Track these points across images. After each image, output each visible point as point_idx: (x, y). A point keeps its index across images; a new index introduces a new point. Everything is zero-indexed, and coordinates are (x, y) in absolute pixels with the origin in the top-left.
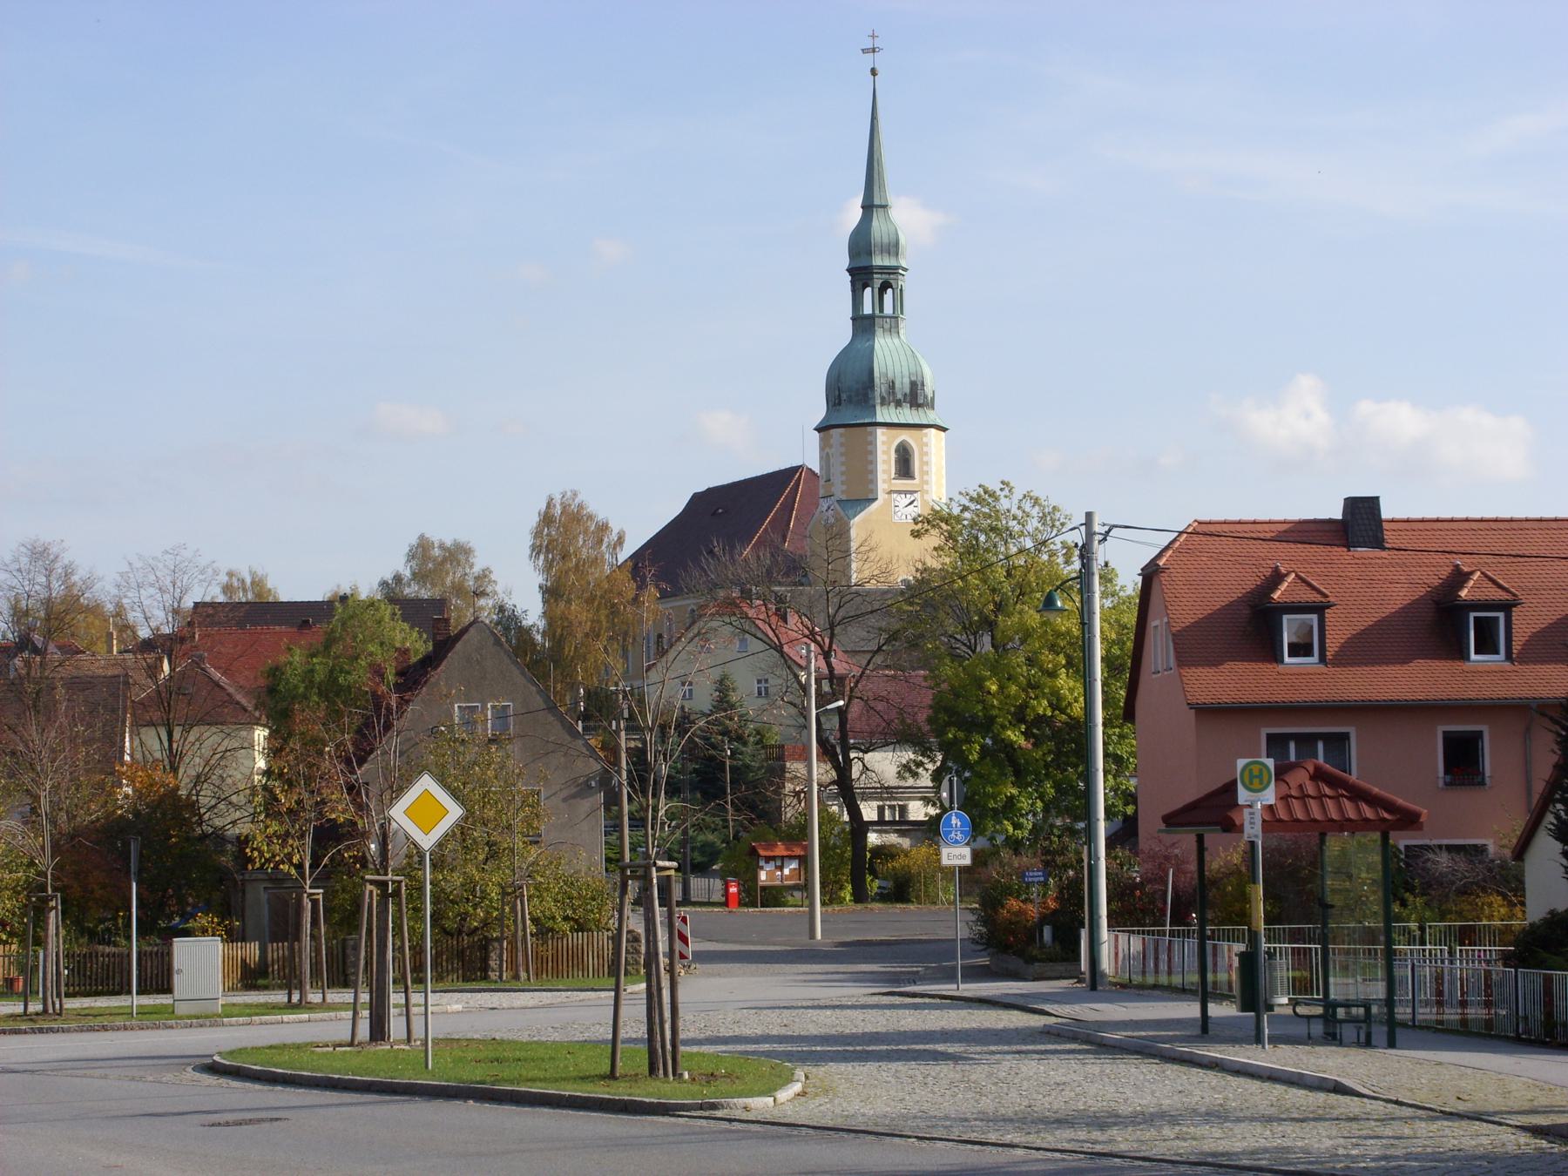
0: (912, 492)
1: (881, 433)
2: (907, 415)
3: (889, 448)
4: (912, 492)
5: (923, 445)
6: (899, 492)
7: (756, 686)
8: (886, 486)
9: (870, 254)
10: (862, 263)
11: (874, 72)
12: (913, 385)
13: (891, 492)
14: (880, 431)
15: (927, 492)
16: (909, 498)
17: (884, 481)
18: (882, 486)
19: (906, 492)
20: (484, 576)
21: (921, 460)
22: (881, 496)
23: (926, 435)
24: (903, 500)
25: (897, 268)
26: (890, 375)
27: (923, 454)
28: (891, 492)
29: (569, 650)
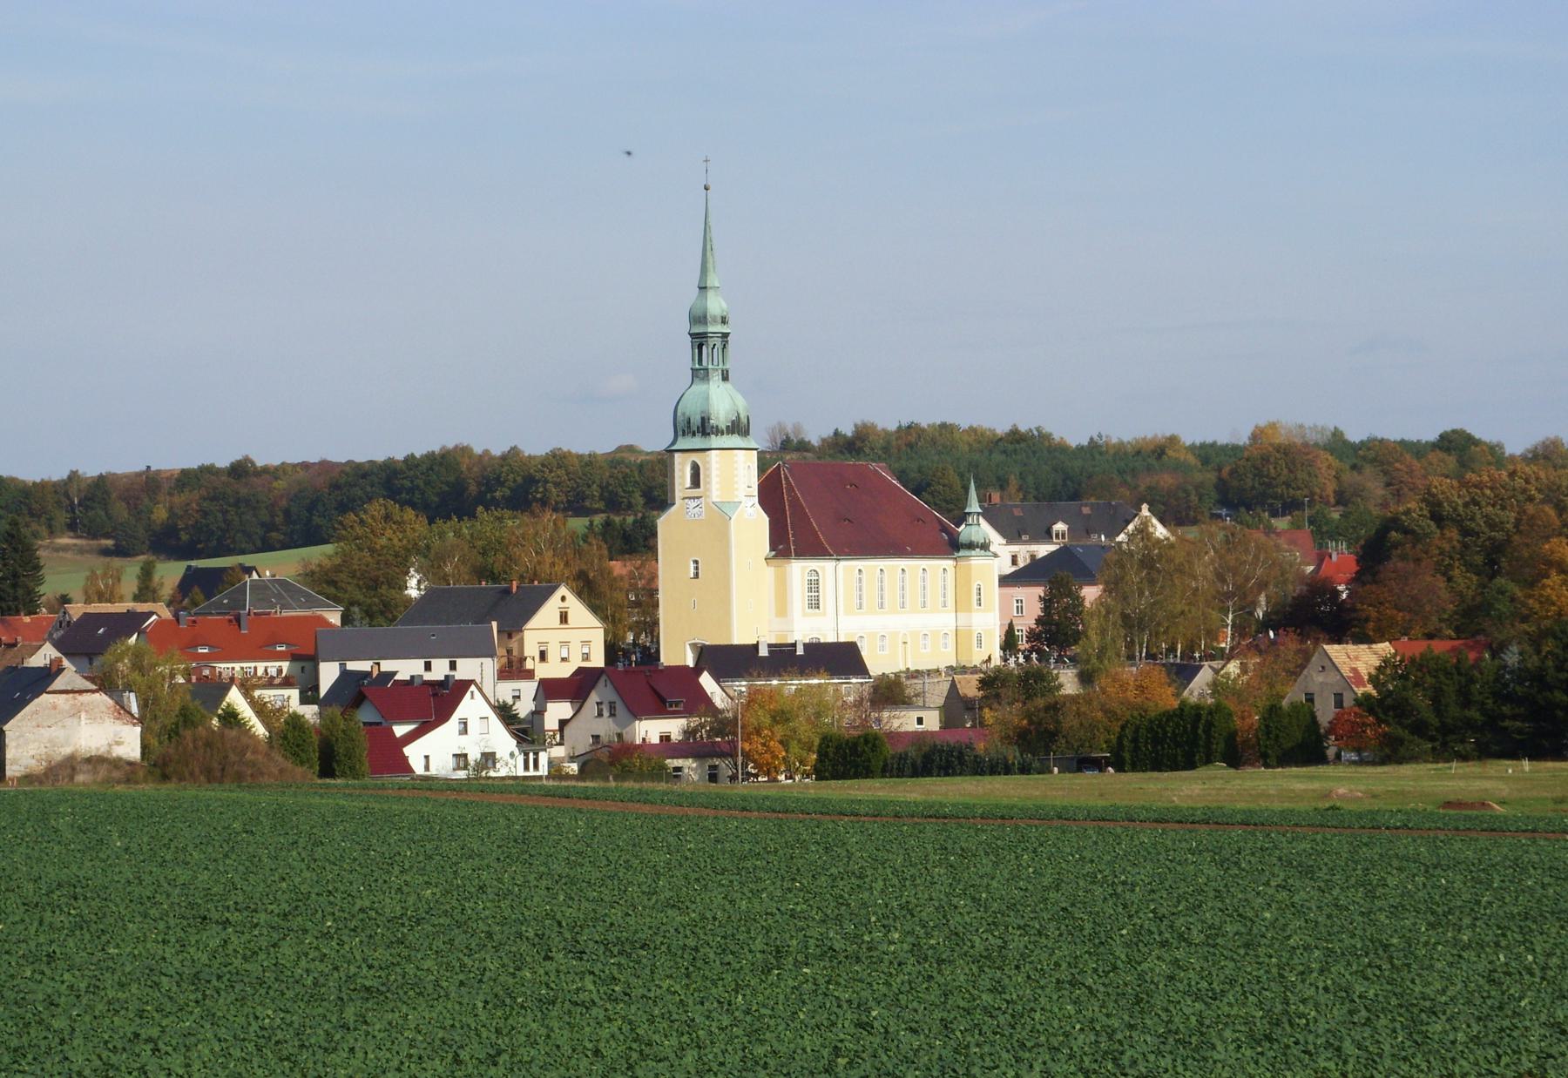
0: (698, 498)
1: (677, 455)
2: (697, 442)
3: (704, 466)
4: (698, 498)
5: (707, 463)
6: (690, 498)
7: (1015, 605)
8: (682, 495)
9: (706, 323)
10: (698, 329)
11: (706, 188)
12: (703, 419)
13: (684, 498)
14: (677, 455)
15: (709, 497)
16: (697, 502)
17: (680, 491)
18: (678, 494)
19: (694, 498)
20: (1322, 428)
21: (705, 475)
22: (678, 501)
23: (736, 455)
24: (692, 504)
25: (706, 333)
26: (687, 414)
27: (707, 469)
28: (684, 498)
29: (1272, 535)
